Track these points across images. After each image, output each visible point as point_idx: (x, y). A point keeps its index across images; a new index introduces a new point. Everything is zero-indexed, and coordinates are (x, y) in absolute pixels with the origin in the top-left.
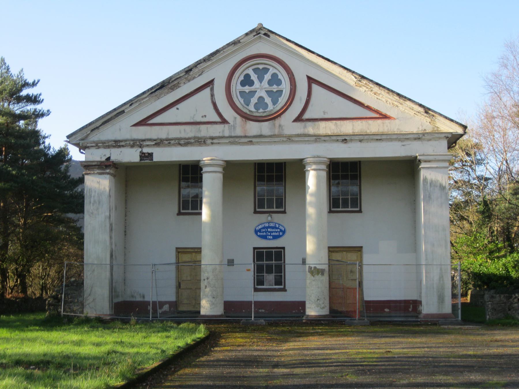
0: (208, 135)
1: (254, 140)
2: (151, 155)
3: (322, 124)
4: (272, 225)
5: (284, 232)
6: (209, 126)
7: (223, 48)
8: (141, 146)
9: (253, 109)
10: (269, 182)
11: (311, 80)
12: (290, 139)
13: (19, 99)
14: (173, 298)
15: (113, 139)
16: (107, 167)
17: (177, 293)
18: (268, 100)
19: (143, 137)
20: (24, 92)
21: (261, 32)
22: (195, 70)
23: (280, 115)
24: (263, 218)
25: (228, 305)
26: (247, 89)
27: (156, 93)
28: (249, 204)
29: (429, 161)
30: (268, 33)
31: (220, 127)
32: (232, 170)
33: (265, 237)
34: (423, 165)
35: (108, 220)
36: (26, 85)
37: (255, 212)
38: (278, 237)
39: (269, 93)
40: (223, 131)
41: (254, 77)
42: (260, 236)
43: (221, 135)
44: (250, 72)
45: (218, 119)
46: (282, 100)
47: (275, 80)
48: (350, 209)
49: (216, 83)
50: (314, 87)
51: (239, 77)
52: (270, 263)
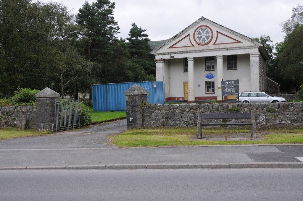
0: (189, 50)
1: (201, 51)
2: (173, 56)
3: (221, 45)
4: (210, 74)
5: (214, 76)
6: (189, 47)
7: (192, 24)
8: (170, 54)
9: (201, 42)
10: (208, 62)
11: (218, 32)
12: (211, 50)
13: (140, 36)
14: (183, 96)
15: (163, 52)
16: (161, 60)
17: (184, 95)
18: (206, 39)
19: (171, 52)
20: (142, 33)
21: (203, 19)
22: (184, 31)
23: (208, 44)
24: (208, 73)
25: (196, 98)
26: (199, 36)
27: (174, 39)
28: (204, 68)
29: (253, 55)
30: (205, 19)
31: (192, 48)
32: (197, 61)
33: (208, 78)
34: (251, 56)
35: (162, 75)
36: (143, 31)
37: (206, 71)
38: (213, 78)
39: (206, 37)
40: (193, 49)
41: (201, 32)
42: (207, 78)
43: (192, 50)
44: (200, 30)
45: (191, 45)
46: (210, 39)
47: (199, 38)
48: (234, 69)
49: (190, 34)
50: (219, 34)
51: (197, 32)
52: (210, 86)
